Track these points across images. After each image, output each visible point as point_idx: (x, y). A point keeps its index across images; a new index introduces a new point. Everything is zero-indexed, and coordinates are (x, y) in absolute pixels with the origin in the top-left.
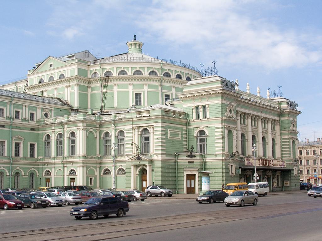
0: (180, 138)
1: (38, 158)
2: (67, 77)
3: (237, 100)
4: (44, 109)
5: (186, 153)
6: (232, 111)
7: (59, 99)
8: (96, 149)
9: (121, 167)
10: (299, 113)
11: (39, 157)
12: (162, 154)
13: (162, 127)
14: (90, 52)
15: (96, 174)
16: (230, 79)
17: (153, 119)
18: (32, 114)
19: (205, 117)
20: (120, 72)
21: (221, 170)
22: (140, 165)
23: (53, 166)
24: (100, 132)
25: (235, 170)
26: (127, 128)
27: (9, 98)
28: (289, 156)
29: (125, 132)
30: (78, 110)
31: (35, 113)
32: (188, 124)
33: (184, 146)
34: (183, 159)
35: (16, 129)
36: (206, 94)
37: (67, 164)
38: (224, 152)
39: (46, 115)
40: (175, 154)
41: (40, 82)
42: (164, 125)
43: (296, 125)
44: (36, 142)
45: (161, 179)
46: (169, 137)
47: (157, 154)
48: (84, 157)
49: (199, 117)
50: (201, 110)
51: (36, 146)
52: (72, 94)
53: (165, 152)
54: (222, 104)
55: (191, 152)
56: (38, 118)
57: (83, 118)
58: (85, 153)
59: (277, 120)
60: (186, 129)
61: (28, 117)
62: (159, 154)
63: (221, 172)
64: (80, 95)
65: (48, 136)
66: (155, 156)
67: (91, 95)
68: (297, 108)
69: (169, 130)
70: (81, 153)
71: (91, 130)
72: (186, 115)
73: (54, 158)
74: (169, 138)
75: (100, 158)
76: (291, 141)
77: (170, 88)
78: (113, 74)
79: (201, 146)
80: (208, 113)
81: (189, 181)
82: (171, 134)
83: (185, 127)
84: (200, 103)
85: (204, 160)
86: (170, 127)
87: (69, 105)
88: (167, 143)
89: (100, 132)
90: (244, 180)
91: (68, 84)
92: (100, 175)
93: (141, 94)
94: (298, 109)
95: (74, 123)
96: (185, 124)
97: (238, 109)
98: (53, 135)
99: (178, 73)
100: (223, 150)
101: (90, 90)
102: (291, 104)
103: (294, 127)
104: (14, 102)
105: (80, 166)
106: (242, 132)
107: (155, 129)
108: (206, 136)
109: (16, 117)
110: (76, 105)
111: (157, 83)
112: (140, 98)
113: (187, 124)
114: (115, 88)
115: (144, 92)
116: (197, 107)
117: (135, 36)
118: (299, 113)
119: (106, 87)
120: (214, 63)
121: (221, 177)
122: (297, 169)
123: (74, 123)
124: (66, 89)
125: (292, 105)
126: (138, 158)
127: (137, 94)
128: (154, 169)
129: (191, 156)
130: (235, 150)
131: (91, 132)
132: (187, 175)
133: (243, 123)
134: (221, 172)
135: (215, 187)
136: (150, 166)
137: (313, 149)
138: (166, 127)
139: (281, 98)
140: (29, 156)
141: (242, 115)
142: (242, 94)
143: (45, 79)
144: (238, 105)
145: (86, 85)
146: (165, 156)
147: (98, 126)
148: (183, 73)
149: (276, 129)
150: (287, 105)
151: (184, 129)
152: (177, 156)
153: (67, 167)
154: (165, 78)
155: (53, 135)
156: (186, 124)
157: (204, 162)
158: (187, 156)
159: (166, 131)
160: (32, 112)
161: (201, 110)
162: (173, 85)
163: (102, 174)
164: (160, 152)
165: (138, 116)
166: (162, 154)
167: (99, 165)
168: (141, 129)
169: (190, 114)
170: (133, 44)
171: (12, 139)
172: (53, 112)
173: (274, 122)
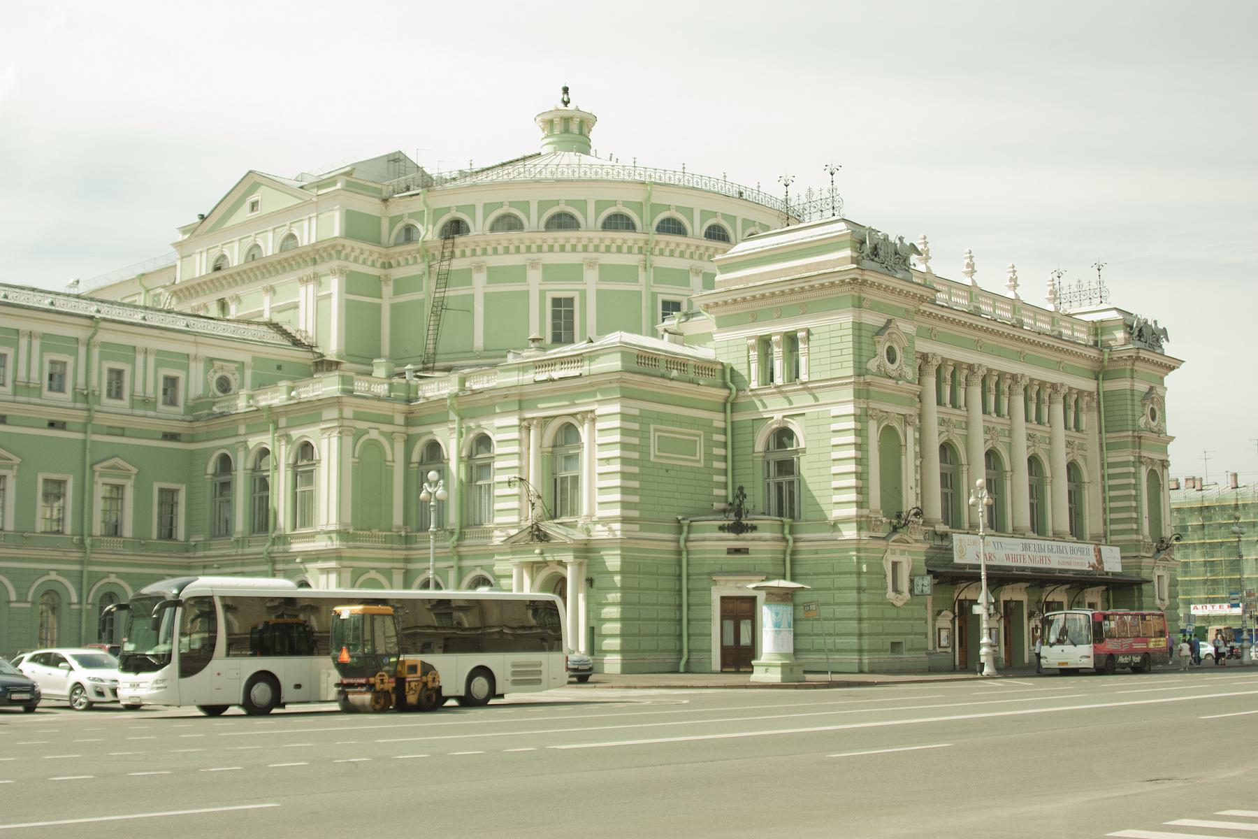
0: (698, 461)
1: (187, 540)
2: (305, 243)
4: (216, 362)
5: (722, 516)
6: (899, 355)
7: (276, 327)
8: (391, 505)
9: (479, 572)
10: (1171, 365)
11: (193, 540)
14: (411, 155)
16: (892, 230)
18: (171, 383)
19: (794, 373)
20: (498, 220)
21: (852, 581)
22: (545, 564)
25: (912, 581)
26: (501, 427)
27: (86, 322)
28: (1137, 532)
29: (494, 438)
30: (338, 363)
31: (127, 368)
32: (730, 406)
33: (717, 492)
34: (711, 542)
35: (108, 434)
36: (796, 287)
37: (284, 562)
38: (865, 512)
39: (224, 385)
40: (679, 521)
41: (217, 269)
42: (635, 408)
43: (1163, 411)
44: (182, 482)
45: (618, 616)
46: (656, 456)
47: (604, 521)
48: (343, 534)
49: (772, 380)
50: (777, 352)
51: (182, 498)
53: (636, 514)
54: (858, 327)
55: (739, 514)
56: (192, 394)
57: (344, 391)
58: (348, 519)
59: (1090, 394)
60: (722, 425)
61: (153, 388)
62: (613, 519)
63: (851, 588)
64: (350, 310)
65: (225, 463)
66: (599, 527)
67: (395, 308)
68: (1164, 344)
69: (655, 430)
70: (334, 518)
71: (374, 434)
72: (728, 377)
74: (652, 459)
75: (407, 539)
76: (1144, 472)
79: (779, 487)
80: (803, 361)
81: (729, 625)
82: (664, 444)
83: (721, 416)
84: (776, 329)
85: (791, 543)
86: (660, 418)
87: (310, 347)
88: (641, 475)
89: (409, 442)
90: (954, 619)
93: (572, 299)
94: (1169, 349)
95: (311, 412)
96: (721, 408)
97: (923, 346)
98: (241, 455)
99: (712, 221)
100: (860, 505)
101: (387, 290)
102: (1140, 331)
103: (1153, 418)
104: (103, 337)
105: (327, 571)
106: (944, 438)
108: (796, 452)
109: (109, 391)
110: (332, 347)
111: (633, 260)
112: (571, 314)
113: (729, 405)
114: (480, 279)
115: (583, 293)
116: (765, 342)
117: (566, 90)
120: (828, 171)
121: (854, 608)
122: (1166, 581)
123: (311, 412)
124: (302, 289)
125: (1146, 336)
126: (539, 535)
127: (557, 302)
128: (595, 576)
129: (738, 528)
130: (910, 501)
131: (374, 443)
132: (723, 599)
133: (993, 408)
134: (851, 588)
135: (822, 647)
136: (580, 564)
138: (644, 418)
140: (155, 535)
141: (988, 381)
142: (938, 287)
144: (930, 335)
145: (376, 272)
146: (637, 527)
149: (1083, 426)
150: (1125, 332)
151: (716, 424)
152: (685, 529)
156: (725, 404)
157: (789, 552)
158: (722, 528)
159: (643, 434)
160: (117, 365)
161: (777, 352)
162: (697, 263)
167: (401, 565)
168: (555, 425)
169: (741, 368)
171: (93, 472)
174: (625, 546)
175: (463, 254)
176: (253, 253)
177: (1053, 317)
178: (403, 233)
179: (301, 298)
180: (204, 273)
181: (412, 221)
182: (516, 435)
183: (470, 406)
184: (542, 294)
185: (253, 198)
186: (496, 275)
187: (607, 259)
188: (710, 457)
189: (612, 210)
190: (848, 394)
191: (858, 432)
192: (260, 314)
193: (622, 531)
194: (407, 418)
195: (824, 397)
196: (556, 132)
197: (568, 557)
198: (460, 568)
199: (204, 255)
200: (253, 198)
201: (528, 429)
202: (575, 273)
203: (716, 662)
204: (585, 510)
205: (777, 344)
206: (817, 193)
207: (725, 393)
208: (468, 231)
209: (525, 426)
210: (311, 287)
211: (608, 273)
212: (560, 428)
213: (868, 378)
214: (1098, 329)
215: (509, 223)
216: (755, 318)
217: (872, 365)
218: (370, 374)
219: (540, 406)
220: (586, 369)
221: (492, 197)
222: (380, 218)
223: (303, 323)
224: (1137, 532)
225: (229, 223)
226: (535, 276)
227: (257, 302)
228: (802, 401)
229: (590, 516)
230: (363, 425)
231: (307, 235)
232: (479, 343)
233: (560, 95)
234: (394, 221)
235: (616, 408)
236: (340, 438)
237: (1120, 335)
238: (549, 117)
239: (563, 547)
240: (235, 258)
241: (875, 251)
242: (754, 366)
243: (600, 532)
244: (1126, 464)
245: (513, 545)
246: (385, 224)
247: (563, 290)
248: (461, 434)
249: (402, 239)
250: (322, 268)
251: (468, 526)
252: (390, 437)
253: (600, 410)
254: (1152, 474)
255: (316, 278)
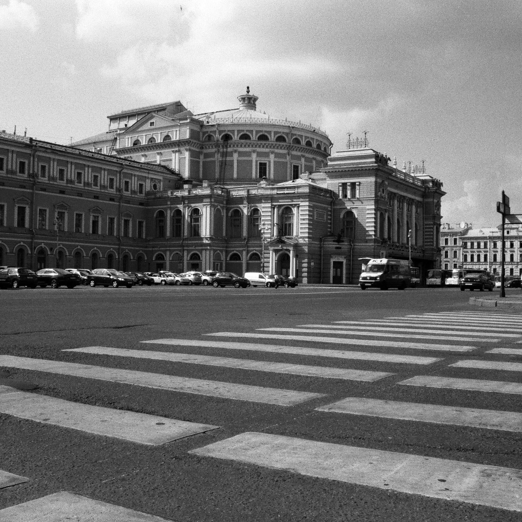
1: (146, 238)
2: (174, 139)
3: (389, 179)
10: (443, 194)
12: (309, 238)
13: (309, 206)
15: (222, 259)
17: (300, 196)
19: (353, 195)
23: (204, 248)
24: (226, 209)
26: (264, 208)
27: (120, 165)
34: (331, 245)
37: (187, 246)
41: (135, 144)
47: (303, 238)
50: (349, 188)
52: (181, 161)
54: (376, 182)
65: (161, 214)
67: (204, 163)
68: (442, 187)
70: (208, 233)
71: (219, 207)
73: (186, 239)
77: (298, 158)
78: (252, 138)
80: (357, 192)
88: (314, 224)
89: (228, 210)
91: (177, 149)
92: (226, 260)
95: (200, 199)
98: (169, 212)
99: (308, 140)
101: (202, 157)
107: (300, 208)
110: (186, 174)
111: (285, 151)
112: (265, 168)
114: (235, 156)
115: (270, 162)
116: (344, 185)
117: (248, 88)
118: (443, 194)
119: (225, 154)
123: (200, 199)
124: (173, 155)
125: (437, 184)
127: (261, 164)
131: (218, 209)
137: (446, 237)
139: (424, 174)
143: (143, 141)
147: (225, 202)
148: (313, 139)
153: (187, 250)
154: (243, 141)
155: (169, 212)
158: (334, 241)
160: (128, 180)
161: (349, 188)
163: (228, 259)
164: (307, 235)
165: (278, 192)
166: (309, 238)
168: (283, 208)
170: (246, 98)
172: (162, 183)
173: (418, 204)
174: (309, 245)
175: (230, 146)
176: (152, 140)
177: (405, 174)
178: (207, 138)
179: (173, 158)
180: (129, 146)
181: (211, 134)
182: (270, 210)
183: (251, 199)
184: (256, 161)
185: (152, 121)
186: (241, 154)
187: (276, 151)
188: (328, 219)
189: (261, 133)
190: (373, 202)
191: (375, 214)
192: (155, 161)
193: (308, 241)
194: (227, 202)
195: (365, 203)
196: (246, 102)
197: (291, 249)
198: (248, 250)
199: (130, 139)
200: (152, 121)
201: (274, 208)
202: (267, 155)
203: (332, 282)
204: (295, 234)
205: (349, 186)
206: (360, 139)
207: (331, 199)
208: (232, 138)
209: (273, 207)
210: (177, 154)
211: (277, 155)
212: (284, 208)
213: (379, 198)
214: (424, 182)
215: (245, 137)
216: (341, 177)
217: (379, 194)
218: (202, 185)
219: (280, 201)
220: (296, 191)
221: (241, 128)
222: (199, 132)
223: (175, 166)
224: (433, 245)
225: (139, 130)
226: (254, 156)
227: (155, 158)
228: (357, 204)
229: (297, 236)
230: (216, 204)
231: (175, 137)
232: (235, 176)
233: (246, 89)
234: (204, 133)
235: (307, 203)
236: (210, 208)
237: (431, 184)
238: (244, 97)
239: (290, 245)
240: (144, 142)
241: (380, 160)
242: (341, 192)
243: (301, 241)
244: (429, 224)
245: (272, 244)
246: (201, 134)
247: (263, 160)
248: (248, 208)
249: (207, 139)
250: (182, 149)
251: (250, 237)
252: (223, 208)
253: (302, 204)
254: (437, 227)
255: (179, 151)
